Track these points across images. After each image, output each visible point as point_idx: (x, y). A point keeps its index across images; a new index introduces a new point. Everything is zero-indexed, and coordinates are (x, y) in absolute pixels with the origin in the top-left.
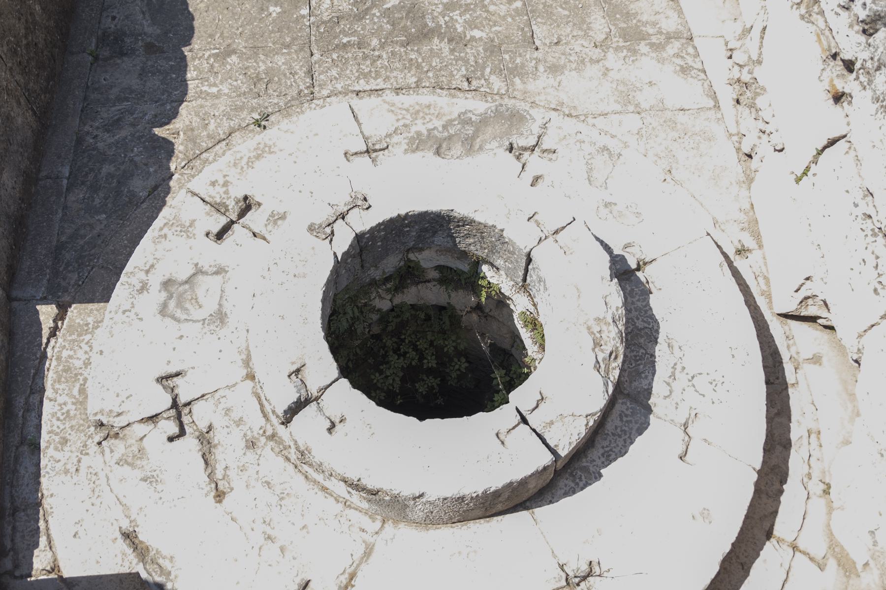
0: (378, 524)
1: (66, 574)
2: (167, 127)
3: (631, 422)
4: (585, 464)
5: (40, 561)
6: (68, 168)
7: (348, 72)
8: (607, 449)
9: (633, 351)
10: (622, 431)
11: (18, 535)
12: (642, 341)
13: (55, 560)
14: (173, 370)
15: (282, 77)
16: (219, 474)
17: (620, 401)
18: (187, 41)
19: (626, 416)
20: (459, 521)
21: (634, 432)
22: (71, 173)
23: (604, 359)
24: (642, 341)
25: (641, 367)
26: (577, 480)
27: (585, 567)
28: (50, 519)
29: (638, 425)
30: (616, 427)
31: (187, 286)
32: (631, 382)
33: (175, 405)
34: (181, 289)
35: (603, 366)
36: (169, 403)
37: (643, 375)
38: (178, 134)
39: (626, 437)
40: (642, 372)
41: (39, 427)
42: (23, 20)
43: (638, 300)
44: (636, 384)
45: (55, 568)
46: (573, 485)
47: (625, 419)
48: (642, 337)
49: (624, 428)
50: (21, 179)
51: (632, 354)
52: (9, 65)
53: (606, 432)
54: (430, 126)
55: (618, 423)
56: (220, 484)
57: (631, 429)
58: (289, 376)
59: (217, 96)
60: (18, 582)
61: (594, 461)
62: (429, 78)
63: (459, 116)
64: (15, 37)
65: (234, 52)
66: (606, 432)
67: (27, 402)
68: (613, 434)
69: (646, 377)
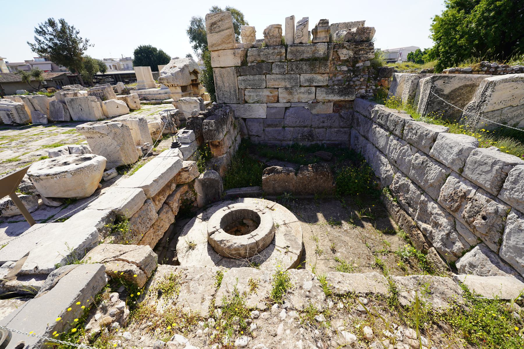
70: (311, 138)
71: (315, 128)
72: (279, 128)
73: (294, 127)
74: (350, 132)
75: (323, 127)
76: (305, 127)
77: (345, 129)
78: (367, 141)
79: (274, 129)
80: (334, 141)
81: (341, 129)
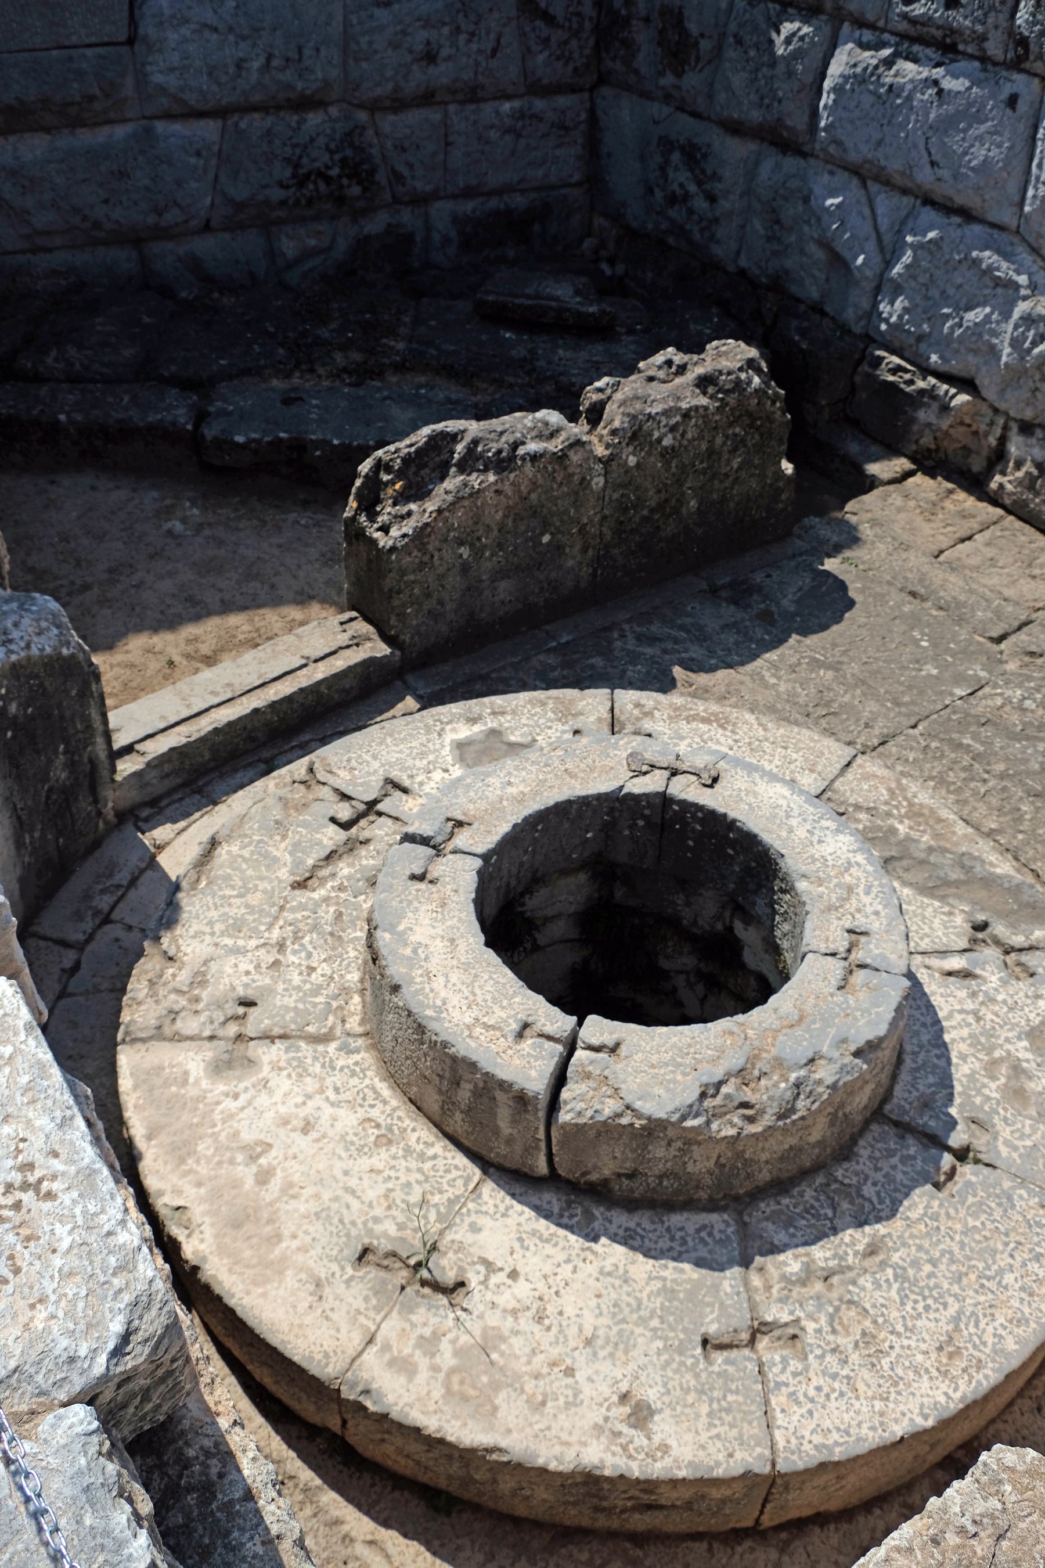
0: (360, 1030)
1: (159, 859)
2: (689, 674)
3: (706, 1244)
4: (597, 1213)
5: (162, 833)
6: (570, 638)
7: (928, 766)
8: (639, 1230)
9: (818, 1200)
10: (682, 1238)
11: (177, 805)
12: (845, 1205)
13: (168, 844)
14: (406, 783)
15: (853, 719)
16: (325, 872)
17: (726, 1217)
18: (805, 632)
19: (710, 1234)
20: (411, 1100)
21: (693, 1255)
22: (567, 643)
23: (728, 1096)
24: (845, 1205)
25: (804, 1222)
26: (566, 1214)
27: (449, 1277)
28: (206, 817)
29: (709, 1256)
30: (682, 1229)
31: (505, 747)
32: (767, 1219)
33: (371, 805)
34: (499, 745)
35: (718, 1100)
36: (369, 797)
37: (792, 1230)
38: (691, 685)
39: (678, 1248)
40: (795, 1227)
41: (290, 762)
42: (663, 496)
43: (905, 1173)
44: (770, 1226)
45: (160, 848)
46: (556, 1210)
47: (704, 1234)
48: (852, 1203)
49: (689, 1239)
50: (520, 606)
51: (812, 1202)
52: (607, 512)
53: (665, 1218)
54: (916, 835)
55: (691, 1228)
56: (314, 880)
57: (695, 1250)
58: (449, 819)
59: (767, 686)
60: (133, 828)
61: (610, 1222)
62: (1015, 837)
63: (963, 854)
64: (638, 498)
65: (837, 670)
66: (665, 1218)
67: (307, 742)
68: (668, 1230)
69: (793, 1236)
70: (356, 190)
71: (374, 107)
72: (100, 136)
73: (220, 113)
74: (592, 112)
75: (427, 98)
76: (304, 104)
77: (562, 101)
78: (791, 163)
79: (65, 141)
80: (499, 192)
81: (539, 104)
